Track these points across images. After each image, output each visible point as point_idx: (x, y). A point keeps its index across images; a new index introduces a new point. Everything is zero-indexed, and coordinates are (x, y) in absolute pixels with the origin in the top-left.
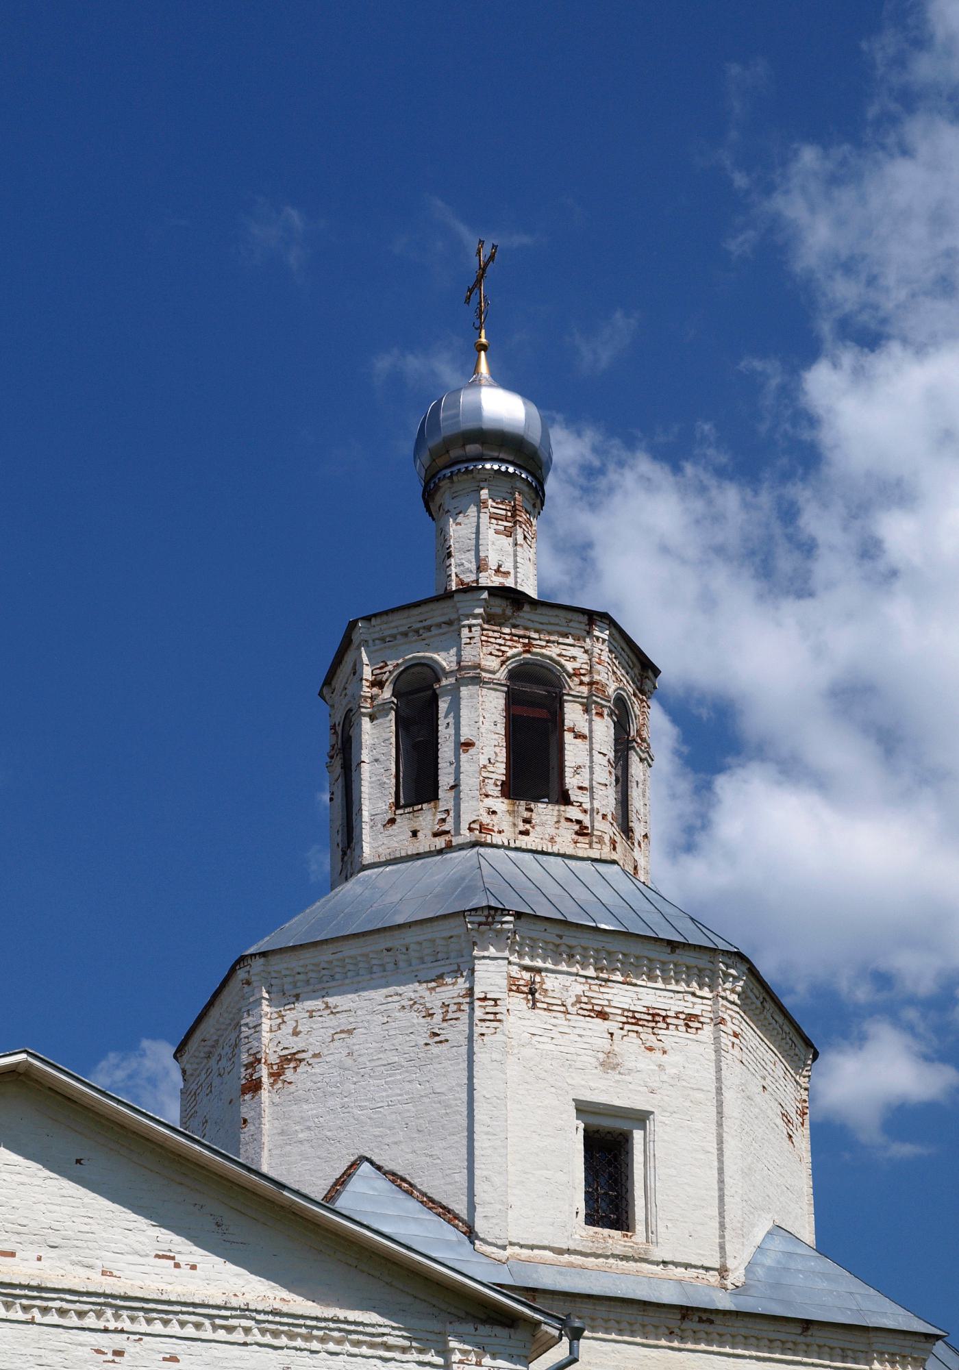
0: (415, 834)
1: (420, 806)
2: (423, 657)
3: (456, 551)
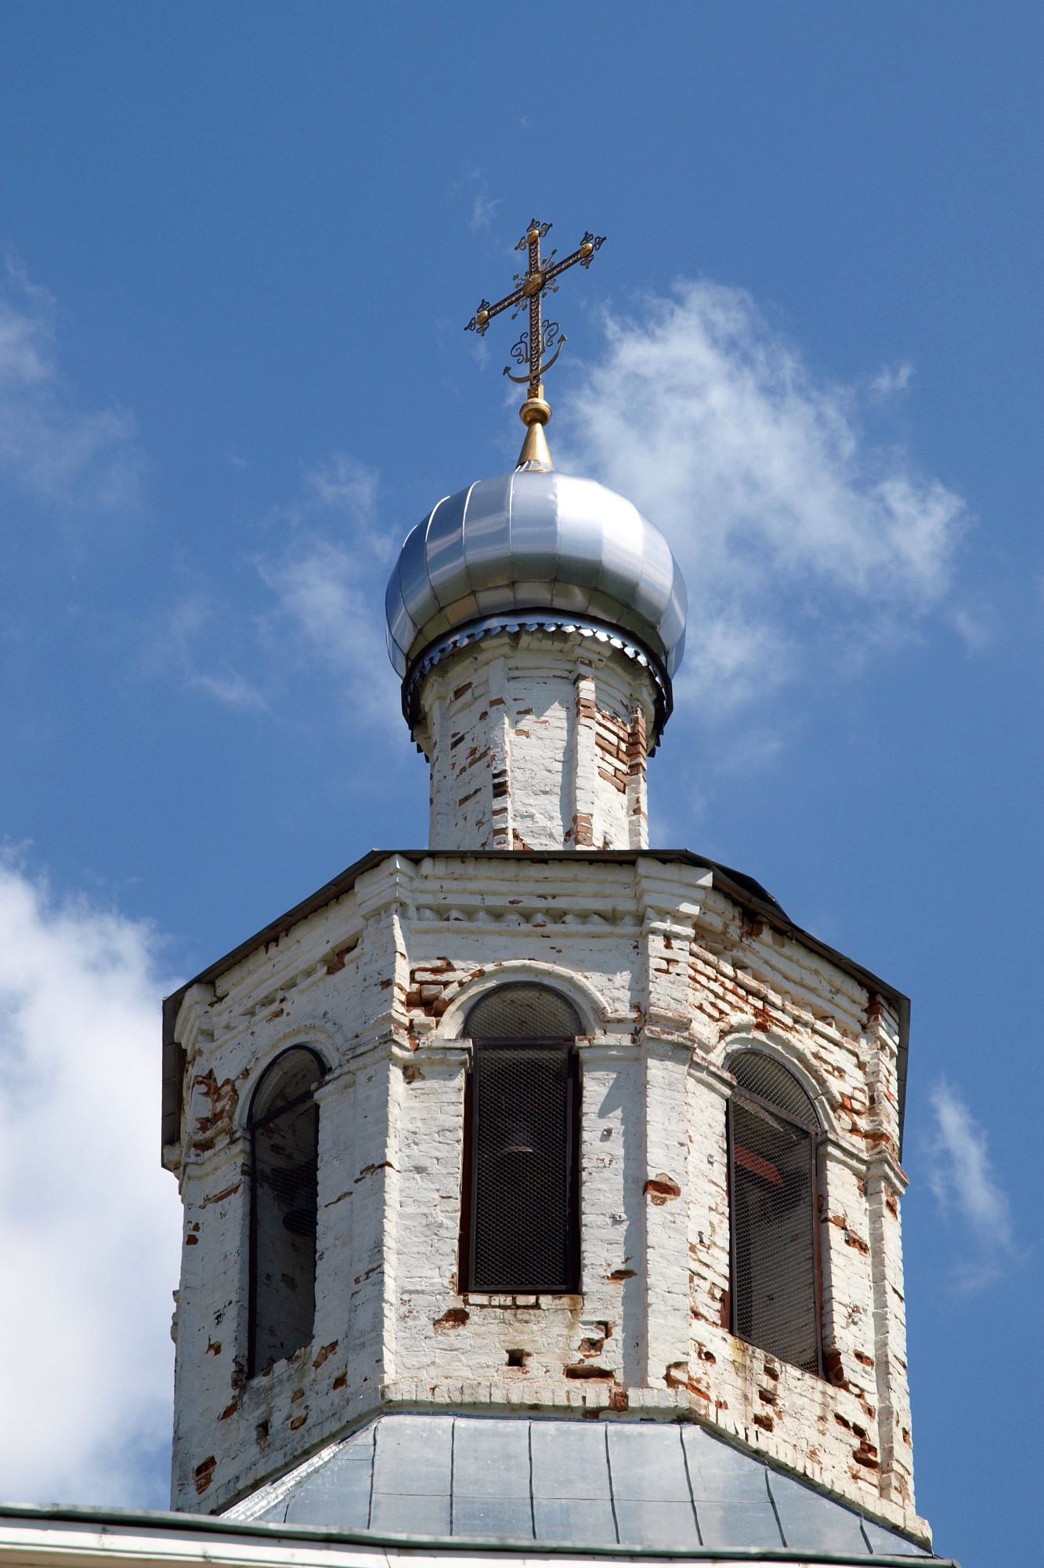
0: (516, 1359)
1: (532, 1299)
2: (549, 973)
3: (516, 785)
